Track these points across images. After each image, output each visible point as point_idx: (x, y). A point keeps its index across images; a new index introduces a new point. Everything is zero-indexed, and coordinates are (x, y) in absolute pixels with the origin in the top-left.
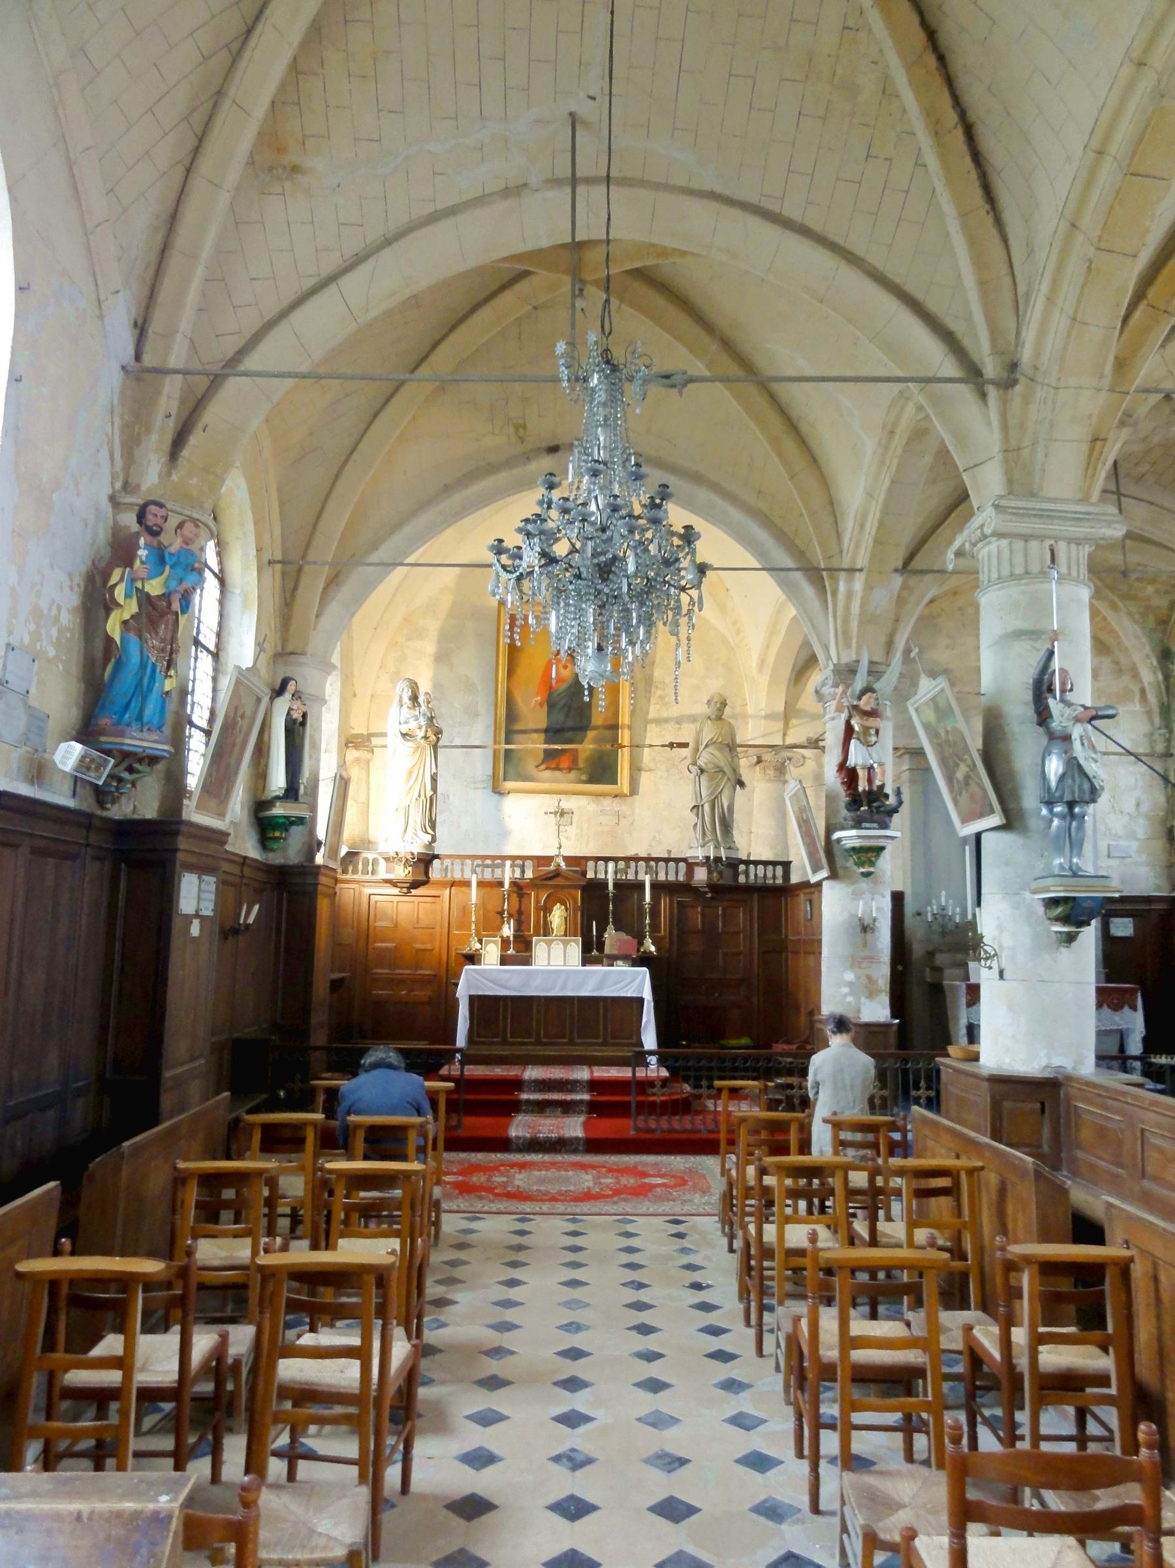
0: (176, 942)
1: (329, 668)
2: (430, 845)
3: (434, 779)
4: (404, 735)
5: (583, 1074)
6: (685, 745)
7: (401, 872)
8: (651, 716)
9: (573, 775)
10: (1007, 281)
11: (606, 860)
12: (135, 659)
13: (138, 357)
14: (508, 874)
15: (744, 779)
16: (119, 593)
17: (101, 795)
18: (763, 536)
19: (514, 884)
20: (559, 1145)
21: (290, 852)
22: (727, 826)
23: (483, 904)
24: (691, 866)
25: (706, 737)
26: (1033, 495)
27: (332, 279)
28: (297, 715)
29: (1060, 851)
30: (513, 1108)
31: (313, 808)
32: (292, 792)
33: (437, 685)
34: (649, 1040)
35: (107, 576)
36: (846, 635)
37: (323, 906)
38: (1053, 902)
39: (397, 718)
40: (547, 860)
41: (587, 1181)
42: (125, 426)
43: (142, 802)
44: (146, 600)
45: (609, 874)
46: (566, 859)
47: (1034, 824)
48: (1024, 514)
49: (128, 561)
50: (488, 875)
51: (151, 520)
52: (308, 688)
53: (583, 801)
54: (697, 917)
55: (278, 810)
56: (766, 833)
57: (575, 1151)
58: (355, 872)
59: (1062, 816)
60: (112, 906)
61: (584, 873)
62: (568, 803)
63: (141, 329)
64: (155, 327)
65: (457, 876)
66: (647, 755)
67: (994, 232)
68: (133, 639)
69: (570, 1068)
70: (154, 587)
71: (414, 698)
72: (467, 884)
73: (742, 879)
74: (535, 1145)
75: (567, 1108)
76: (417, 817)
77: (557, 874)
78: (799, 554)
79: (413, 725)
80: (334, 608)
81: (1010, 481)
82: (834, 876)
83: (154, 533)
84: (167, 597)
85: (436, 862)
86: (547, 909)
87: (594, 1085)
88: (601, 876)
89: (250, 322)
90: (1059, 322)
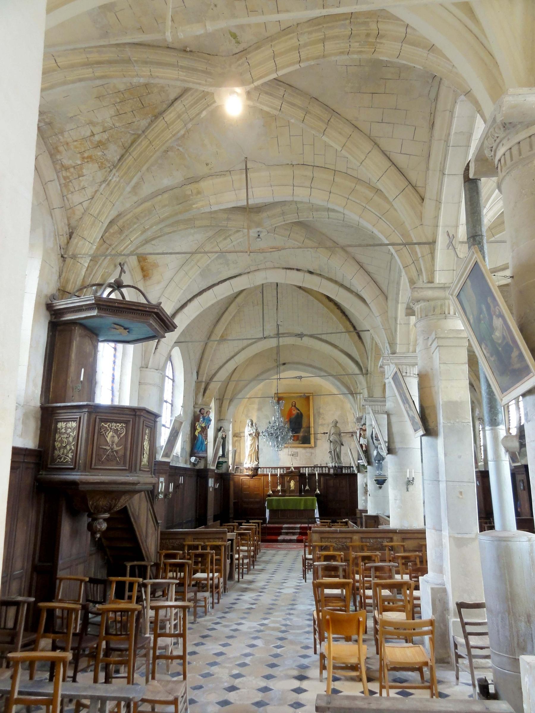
0: (209, 492)
1: (230, 422)
2: (257, 465)
3: (258, 446)
4: (249, 435)
5: (299, 526)
6: (327, 433)
7: (250, 473)
8: (320, 423)
9: (298, 442)
10: (365, 354)
11: (306, 467)
12: (201, 439)
13: (197, 379)
14: (279, 472)
15: (343, 443)
16: (198, 427)
17: (194, 464)
18: (338, 383)
19: (281, 475)
20: (290, 541)
21: (223, 470)
22: (339, 458)
23: (272, 481)
24: (329, 469)
25: (332, 432)
26: (372, 397)
27: (233, 357)
28: (224, 436)
29: (378, 470)
30: (280, 534)
31: (228, 459)
32: (223, 455)
33: (258, 418)
34: (317, 515)
35: (195, 424)
36: (360, 408)
37: (232, 483)
38: (375, 480)
39: (248, 430)
40: (288, 468)
41: (295, 546)
42: (196, 392)
43: (201, 466)
44: (202, 427)
45: (307, 471)
46: (294, 467)
47: (374, 464)
48: (371, 401)
49: (199, 421)
50: (273, 473)
51: (202, 412)
52: (226, 428)
53: (301, 449)
54: (331, 483)
55: (220, 460)
56: (350, 457)
57: (294, 542)
58: (238, 472)
59: (378, 463)
60: (197, 485)
61: (300, 471)
62: (295, 450)
63: (198, 373)
64: (200, 373)
65: (265, 473)
66: (319, 436)
67: (361, 345)
68: (200, 435)
70: (203, 425)
71: (252, 424)
72: (268, 475)
73: (344, 472)
74: (284, 541)
75: (294, 534)
76: (254, 457)
77: (292, 472)
78: (348, 388)
79: (252, 432)
80: (231, 407)
81: (369, 393)
82: (359, 471)
83: (202, 414)
84: (205, 427)
85: (259, 469)
86: (289, 482)
87: (301, 528)
88: (304, 472)
89: (217, 367)
90: (373, 365)
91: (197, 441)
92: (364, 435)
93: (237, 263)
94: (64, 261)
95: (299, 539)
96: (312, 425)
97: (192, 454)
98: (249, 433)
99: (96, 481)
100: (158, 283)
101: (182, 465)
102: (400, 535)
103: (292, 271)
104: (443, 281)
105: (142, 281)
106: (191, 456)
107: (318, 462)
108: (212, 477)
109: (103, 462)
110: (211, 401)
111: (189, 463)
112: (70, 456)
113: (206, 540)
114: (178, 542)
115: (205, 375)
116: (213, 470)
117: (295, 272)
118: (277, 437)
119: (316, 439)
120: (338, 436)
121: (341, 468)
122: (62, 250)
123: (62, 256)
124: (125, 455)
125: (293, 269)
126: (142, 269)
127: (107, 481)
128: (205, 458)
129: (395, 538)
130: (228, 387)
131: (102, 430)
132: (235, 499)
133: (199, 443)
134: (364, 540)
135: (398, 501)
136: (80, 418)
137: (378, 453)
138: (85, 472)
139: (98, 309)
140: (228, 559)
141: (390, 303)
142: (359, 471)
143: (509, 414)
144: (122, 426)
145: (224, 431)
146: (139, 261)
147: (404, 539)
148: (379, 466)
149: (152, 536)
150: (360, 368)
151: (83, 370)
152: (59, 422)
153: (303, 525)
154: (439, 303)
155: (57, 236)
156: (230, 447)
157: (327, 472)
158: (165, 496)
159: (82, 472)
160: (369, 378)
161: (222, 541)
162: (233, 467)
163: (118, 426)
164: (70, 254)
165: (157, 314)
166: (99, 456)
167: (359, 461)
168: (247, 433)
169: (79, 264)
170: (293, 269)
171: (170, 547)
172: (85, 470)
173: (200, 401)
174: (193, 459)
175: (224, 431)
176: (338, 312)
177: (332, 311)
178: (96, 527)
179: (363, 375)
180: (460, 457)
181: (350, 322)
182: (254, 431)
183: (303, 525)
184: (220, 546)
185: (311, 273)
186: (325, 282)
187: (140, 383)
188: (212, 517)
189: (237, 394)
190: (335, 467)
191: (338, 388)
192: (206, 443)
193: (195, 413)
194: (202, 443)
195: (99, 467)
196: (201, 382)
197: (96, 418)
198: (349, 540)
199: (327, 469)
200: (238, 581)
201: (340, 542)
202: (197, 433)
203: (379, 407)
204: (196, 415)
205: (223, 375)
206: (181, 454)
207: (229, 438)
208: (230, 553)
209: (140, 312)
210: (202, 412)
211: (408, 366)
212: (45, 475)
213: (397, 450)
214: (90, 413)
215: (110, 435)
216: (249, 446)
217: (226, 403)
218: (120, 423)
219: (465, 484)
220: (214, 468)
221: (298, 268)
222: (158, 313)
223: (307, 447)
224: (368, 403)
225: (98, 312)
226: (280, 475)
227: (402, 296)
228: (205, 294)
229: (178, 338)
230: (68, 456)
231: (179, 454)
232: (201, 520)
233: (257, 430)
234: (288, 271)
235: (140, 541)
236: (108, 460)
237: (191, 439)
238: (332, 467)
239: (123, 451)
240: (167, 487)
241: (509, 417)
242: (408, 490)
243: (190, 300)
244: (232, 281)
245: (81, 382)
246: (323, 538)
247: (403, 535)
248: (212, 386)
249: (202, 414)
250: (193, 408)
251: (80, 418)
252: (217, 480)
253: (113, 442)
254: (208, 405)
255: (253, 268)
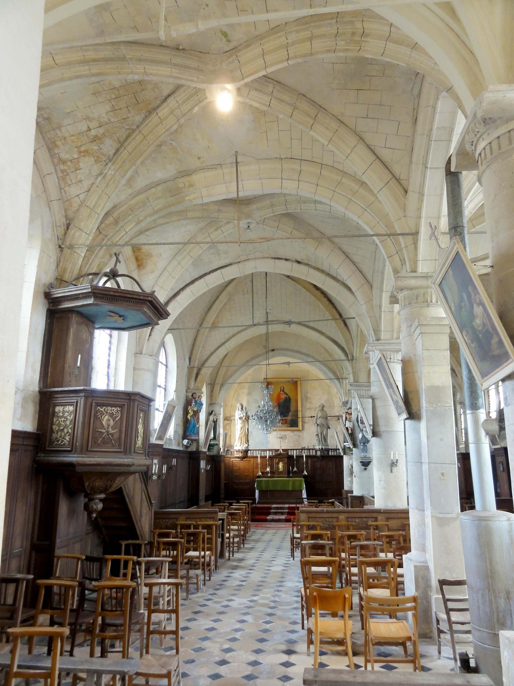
0: (201, 473)
1: (221, 406)
2: (247, 447)
3: (248, 429)
4: (240, 418)
5: (287, 506)
6: (314, 417)
7: (240, 455)
8: (307, 407)
9: (286, 425)
10: (351, 341)
11: (294, 450)
12: (193, 422)
13: (190, 364)
14: (268, 454)
15: (330, 427)
16: (190, 411)
17: (187, 447)
18: (325, 369)
19: (270, 457)
20: (279, 521)
21: (214, 452)
22: (326, 440)
23: (262, 463)
24: (316, 451)
25: (319, 415)
26: (358, 382)
27: (223, 344)
28: (215, 420)
29: (363, 452)
30: (269, 514)
31: (219, 442)
32: (214, 438)
33: (248, 402)
34: (304, 495)
35: (187, 408)
36: (346, 393)
37: (222, 465)
38: (361, 462)
39: (238, 414)
40: (277, 450)
41: (283, 526)
42: (188, 377)
43: (193, 448)
44: (194, 411)
45: (295, 453)
46: (282, 450)
47: (359, 447)
48: (356, 386)
49: (191, 405)
50: (263, 455)
51: (194, 396)
52: (217, 412)
53: (289, 432)
54: (318, 464)
55: (212, 443)
56: (336, 440)
57: (283, 522)
58: (228, 455)
59: (363, 446)
60: (189, 467)
61: (288, 453)
62: (283, 433)
63: (190, 359)
64: (192, 359)
65: (255, 455)
66: (306, 419)
67: (347, 332)
68: (192, 419)
69: (92, 369)
70: (195, 409)
71: (242, 408)
72: (258, 457)
73: (330, 454)
74: (273, 520)
75: (282, 513)
76: (244, 440)
77: (280, 454)
78: (334, 373)
79: (242, 416)
80: (222, 392)
81: (354, 378)
82: (345, 454)
83: (195, 398)
84: (197, 410)
85: (249, 451)
86: (278, 464)
87: (289, 508)
88: (292, 454)
89: (208, 353)
90: (358, 351)
91: (189, 424)
92: (350, 418)
93: (228, 253)
94: (62, 251)
95: (287, 518)
96: (300, 408)
97: (184, 437)
98: (239, 416)
99: (92, 463)
100: (152, 272)
101: (175, 447)
102: (384, 515)
103: (281, 261)
104: (425, 270)
105: (137, 270)
106: (184, 438)
107: (305, 445)
108: (203, 459)
109: (98, 444)
110: (203, 385)
111: (181, 445)
112: (68, 439)
113: (198, 520)
114: (171, 521)
115: (197, 361)
116: (205, 453)
117: (284, 261)
118: (266, 421)
119: (303, 423)
120: (325, 420)
121: (328, 450)
122: (60, 240)
123: (60, 247)
124: (120, 438)
125: (282, 259)
126: (137, 259)
127: (103, 463)
128: (197, 441)
129: (380, 518)
130: (219, 372)
131: (98, 414)
132: (225, 480)
133: (191, 426)
134: (349, 520)
135: (382, 482)
136: (77, 402)
137: (363, 436)
138: (82, 454)
139: (94, 297)
140: (219, 538)
141: (374, 291)
142: (345, 454)
143: (489, 398)
144: (117, 410)
145: (215, 415)
146: (134, 252)
147: (388, 519)
148: (364, 448)
149: (146, 516)
150: (346, 354)
151: (80, 356)
152: (57, 406)
153: (291, 505)
154: (422, 291)
155: (55, 227)
156: (221, 430)
157: (314, 454)
158: (159, 477)
159: (79, 454)
160: (354, 363)
161: (213, 521)
162: (224, 450)
163: (114, 410)
164: (68, 244)
165: (151, 302)
166: (95, 439)
167: (345, 444)
168: (237, 417)
169: (76, 254)
170: (282, 259)
171: (164, 526)
172: (81, 452)
173: (192, 386)
174: (185, 442)
175: (215, 415)
176: (325, 300)
177: (319, 300)
178: (92, 507)
179: (349, 361)
180: (442, 440)
181: (336, 309)
182: (244, 414)
183: (291, 505)
184: (212, 525)
185: (299, 262)
186: (312, 271)
187: (134, 369)
188: (204, 497)
189: (228, 379)
190: (322, 449)
191: (325, 373)
192: (198, 426)
193: (187, 397)
194: (194, 426)
195: (96, 449)
196: (193, 367)
197: (92, 402)
198: (335, 520)
199: (314, 451)
200: (229, 559)
201: (326, 521)
202: (189, 417)
203: (364, 391)
204: (189, 399)
205: (214, 361)
206: (174, 437)
207: (220, 421)
208: (221, 532)
209: (134, 300)
210: (194, 396)
211: (392, 353)
212: (44, 457)
213: (381, 433)
214: (86, 397)
215: (105, 419)
216: (239, 429)
217: (217, 388)
218: (115, 407)
219: (447, 466)
220: (205, 450)
221: (287, 258)
222: (151, 301)
223: (295, 430)
224: (354, 388)
225: (94, 300)
226: (269, 457)
227: (386, 285)
228: (197, 283)
229: (171, 325)
230: (65, 439)
231: (172, 437)
232: (193, 500)
233: (246, 413)
234: (276, 261)
235: (134, 521)
236: (104, 442)
237: (184, 422)
238: (319, 450)
239: (118, 434)
240: (160, 469)
241: (489, 401)
242: (392, 472)
243: (183, 289)
244: (223, 270)
245: (78, 367)
246: (310, 517)
247: (387, 514)
248: (204, 371)
249: (195, 398)
250: (185, 392)
251: (77, 402)
252: (208, 462)
253: (108, 425)
254: (200, 389)
255: (243, 258)
